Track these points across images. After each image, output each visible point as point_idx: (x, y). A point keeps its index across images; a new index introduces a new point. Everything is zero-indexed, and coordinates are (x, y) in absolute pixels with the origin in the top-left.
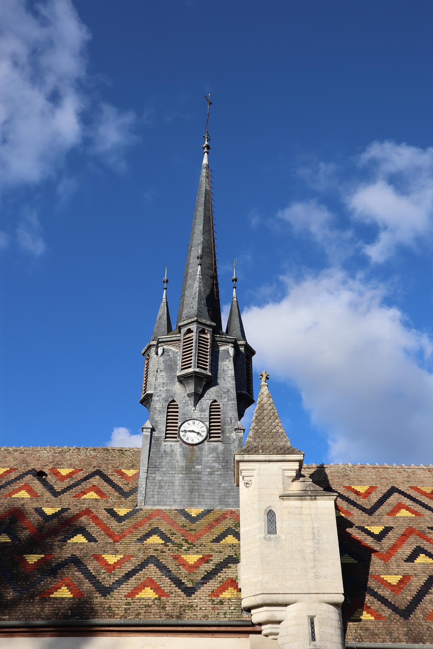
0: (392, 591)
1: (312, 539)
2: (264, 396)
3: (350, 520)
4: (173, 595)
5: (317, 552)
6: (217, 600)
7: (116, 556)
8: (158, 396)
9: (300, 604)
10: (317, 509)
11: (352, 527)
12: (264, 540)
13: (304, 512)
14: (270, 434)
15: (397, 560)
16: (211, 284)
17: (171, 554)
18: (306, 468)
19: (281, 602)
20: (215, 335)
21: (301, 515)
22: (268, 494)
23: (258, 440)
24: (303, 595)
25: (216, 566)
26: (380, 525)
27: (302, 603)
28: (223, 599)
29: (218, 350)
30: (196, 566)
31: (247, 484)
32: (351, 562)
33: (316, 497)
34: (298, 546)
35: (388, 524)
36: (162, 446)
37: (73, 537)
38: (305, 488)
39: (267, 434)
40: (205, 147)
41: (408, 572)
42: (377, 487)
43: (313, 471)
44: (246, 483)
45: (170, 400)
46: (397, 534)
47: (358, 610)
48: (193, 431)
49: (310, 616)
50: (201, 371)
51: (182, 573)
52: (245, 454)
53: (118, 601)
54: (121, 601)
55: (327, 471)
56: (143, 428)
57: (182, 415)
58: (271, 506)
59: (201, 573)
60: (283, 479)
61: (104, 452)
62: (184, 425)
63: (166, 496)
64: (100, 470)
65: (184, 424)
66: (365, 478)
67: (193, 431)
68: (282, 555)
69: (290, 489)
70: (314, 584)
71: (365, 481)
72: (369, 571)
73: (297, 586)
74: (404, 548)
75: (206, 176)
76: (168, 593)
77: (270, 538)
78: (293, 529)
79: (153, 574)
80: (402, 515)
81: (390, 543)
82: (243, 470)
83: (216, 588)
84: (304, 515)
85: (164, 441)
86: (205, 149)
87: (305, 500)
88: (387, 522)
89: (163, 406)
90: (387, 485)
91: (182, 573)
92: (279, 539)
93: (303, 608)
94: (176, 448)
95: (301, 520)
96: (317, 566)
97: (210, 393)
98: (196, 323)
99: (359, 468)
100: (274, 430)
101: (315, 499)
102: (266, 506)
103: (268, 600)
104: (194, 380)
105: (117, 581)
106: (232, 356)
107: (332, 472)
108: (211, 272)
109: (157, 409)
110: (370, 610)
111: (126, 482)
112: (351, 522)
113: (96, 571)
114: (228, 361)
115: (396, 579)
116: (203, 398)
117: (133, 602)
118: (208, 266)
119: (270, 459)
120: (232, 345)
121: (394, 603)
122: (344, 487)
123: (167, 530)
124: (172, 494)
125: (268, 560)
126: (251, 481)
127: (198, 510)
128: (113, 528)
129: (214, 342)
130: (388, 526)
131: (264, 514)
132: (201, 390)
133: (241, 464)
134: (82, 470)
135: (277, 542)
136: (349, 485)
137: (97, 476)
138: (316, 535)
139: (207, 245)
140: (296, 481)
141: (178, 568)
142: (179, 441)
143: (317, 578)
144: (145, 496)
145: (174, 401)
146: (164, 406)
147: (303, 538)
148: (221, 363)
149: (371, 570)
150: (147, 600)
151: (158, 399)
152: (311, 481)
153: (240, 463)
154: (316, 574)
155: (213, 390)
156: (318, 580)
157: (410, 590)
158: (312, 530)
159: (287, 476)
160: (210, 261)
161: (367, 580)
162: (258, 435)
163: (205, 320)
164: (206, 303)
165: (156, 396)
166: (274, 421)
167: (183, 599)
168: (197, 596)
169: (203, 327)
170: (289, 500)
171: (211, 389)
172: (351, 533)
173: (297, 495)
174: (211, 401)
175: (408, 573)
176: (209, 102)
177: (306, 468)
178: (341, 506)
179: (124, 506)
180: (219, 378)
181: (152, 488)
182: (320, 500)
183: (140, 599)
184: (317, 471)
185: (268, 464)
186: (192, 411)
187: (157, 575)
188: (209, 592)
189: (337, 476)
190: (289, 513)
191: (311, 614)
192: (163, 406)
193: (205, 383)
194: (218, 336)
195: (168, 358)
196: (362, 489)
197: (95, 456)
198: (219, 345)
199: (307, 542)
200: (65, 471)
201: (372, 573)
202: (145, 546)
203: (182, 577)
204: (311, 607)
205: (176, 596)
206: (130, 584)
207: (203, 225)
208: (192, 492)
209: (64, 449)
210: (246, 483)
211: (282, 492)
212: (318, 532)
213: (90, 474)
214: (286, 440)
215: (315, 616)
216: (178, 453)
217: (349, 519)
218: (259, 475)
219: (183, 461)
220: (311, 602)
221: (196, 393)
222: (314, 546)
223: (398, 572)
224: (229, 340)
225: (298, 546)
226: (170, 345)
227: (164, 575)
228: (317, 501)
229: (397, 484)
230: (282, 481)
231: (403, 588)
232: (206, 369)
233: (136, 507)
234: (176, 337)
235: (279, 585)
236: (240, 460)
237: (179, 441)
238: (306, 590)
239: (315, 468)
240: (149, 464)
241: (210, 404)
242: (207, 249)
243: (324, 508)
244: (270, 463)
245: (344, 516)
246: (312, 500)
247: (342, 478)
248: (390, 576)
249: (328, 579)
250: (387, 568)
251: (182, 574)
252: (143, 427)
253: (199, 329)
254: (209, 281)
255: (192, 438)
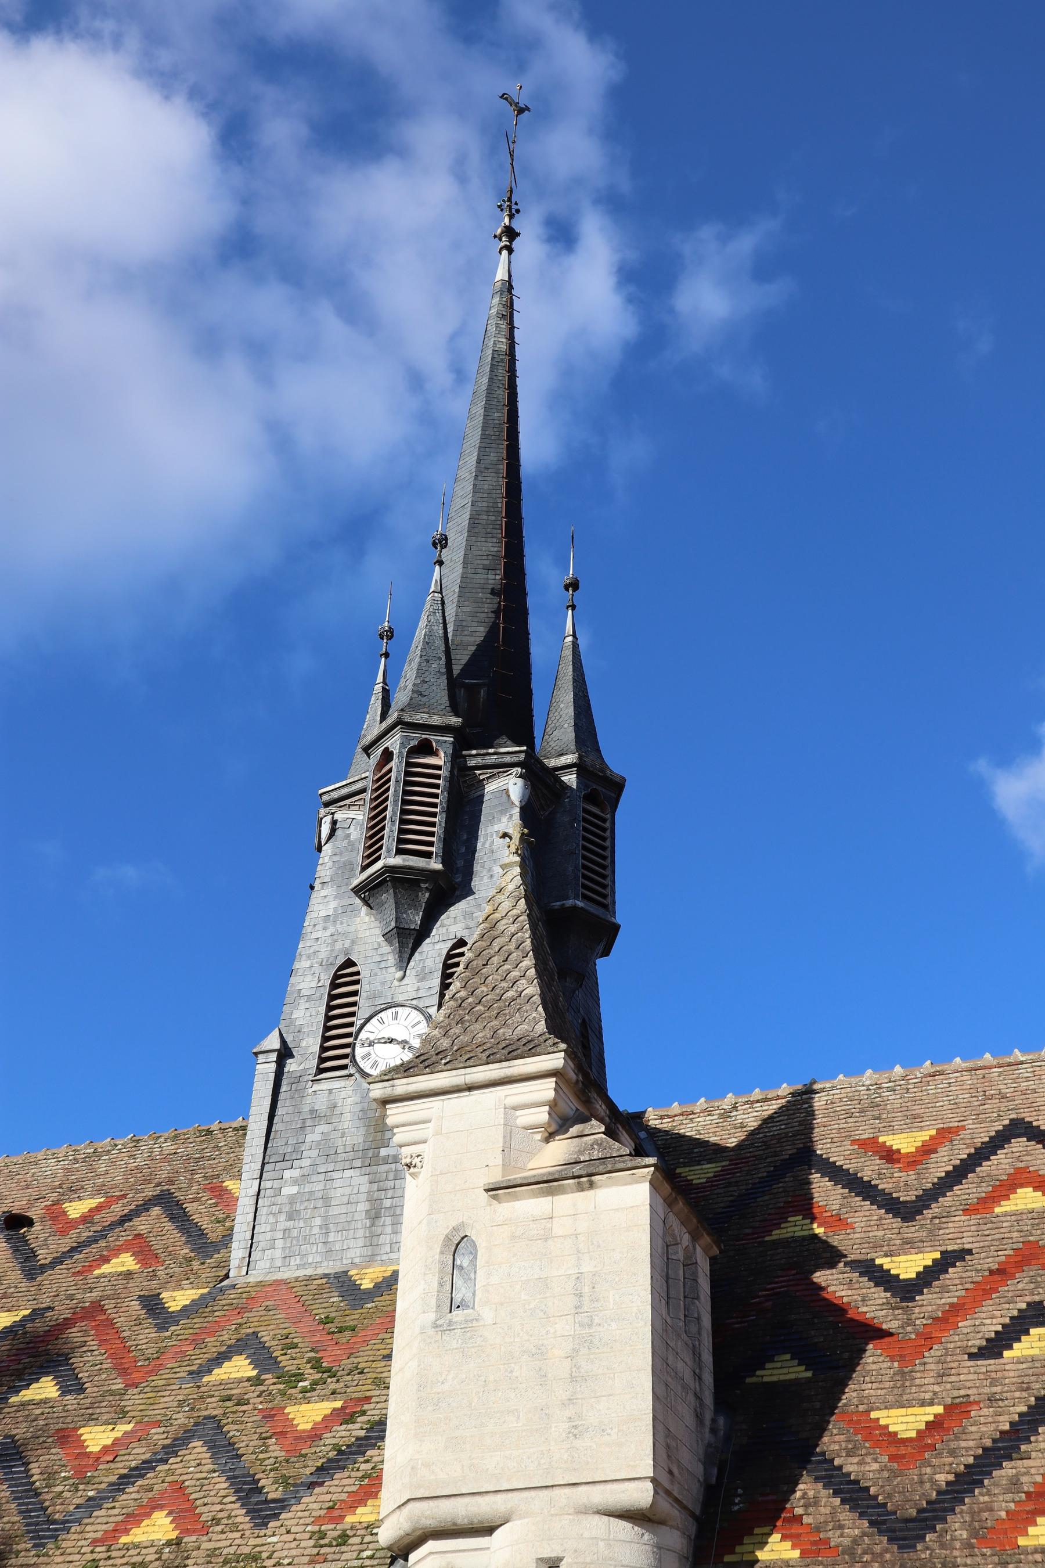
0: (892, 1458)
1: (573, 1311)
2: (503, 897)
3: (835, 1244)
4: (219, 1528)
5: (584, 1351)
6: (332, 1531)
7: (114, 1429)
8: (309, 957)
9: (519, 1522)
10: (596, 1214)
11: (832, 1265)
12: (431, 1332)
13: (558, 1230)
14: (495, 1005)
15: (946, 1354)
16: (492, 612)
17: (260, 1407)
18: (758, 1101)
19: (466, 1521)
20: (464, 753)
21: (546, 1240)
22: (458, 1188)
23: (457, 1030)
24: (533, 1493)
25: (368, 1430)
26: (929, 1249)
27: (526, 1520)
28: (352, 1529)
29: (479, 793)
30: (315, 1435)
31: (410, 1167)
32: (792, 1376)
33: (593, 1178)
34: (529, 1340)
35: (958, 1241)
36: (307, 1095)
37: (27, 1386)
38: (576, 1156)
39: (486, 1006)
40: (500, 235)
41: (969, 1392)
42: (963, 1128)
43: (775, 1107)
44: (407, 1165)
45: (341, 960)
46: (977, 1271)
47: (757, 1531)
48: (391, 1041)
49: (546, 1559)
50: (407, 863)
51: (269, 1458)
52: (397, 1076)
53: (67, 1560)
54: (75, 1559)
55: (819, 1102)
56: (256, 1054)
57: (367, 998)
58: (462, 1225)
59: (320, 1454)
60: (504, 1137)
61: (198, 1139)
62: (368, 1027)
63: (305, 1239)
64: (169, 1190)
65: (368, 1025)
66: (933, 1105)
67: (391, 1041)
68: (480, 1372)
69: (530, 1166)
70: (565, 1456)
71: (928, 1115)
72: (840, 1400)
73: (515, 1464)
74: (983, 1315)
75: (498, 313)
76: (208, 1521)
77: (450, 1323)
78: (518, 1287)
79: (192, 1469)
80: (1014, 1208)
81: (943, 1301)
82: (398, 1127)
83: (344, 1496)
84: (556, 1239)
85: (312, 1081)
86: (504, 239)
87: (562, 1191)
88: (960, 1235)
89: (319, 981)
90: (999, 1116)
91: (269, 1458)
92: (475, 1324)
93: (527, 1535)
94: (343, 1095)
95: (545, 1255)
96: (580, 1397)
97: (446, 922)
98: (401, 728)
99: (926, 1076)
100: (511, 994)
101: (591, 1185)
102: (448, 1227)
103: (426, 1518)
104: (391, 891)
105: (90, 1499)
106: (517, 803)
107: (832, 1103)
108: (493, 577)
109: (304, 992)
110: (796, 1529)
111: (223, 1213)
112: (839, 1251)
113: (45, 1476)
114: (505, 819)
115: (919, 1418)
116: (428, 941)
117: (105, 1559)
118: (487, 562)
119: (467, 1082)
120: (519, 769)
121: (885, 1498)
122: (854, 1142)
123: (279, 1336)
124: (323, 1232)
125: (438, 1393)
126: (420, 1155)
127: (384, 1269)
128: (139, 1347)
129: (467, 773)
130: (956, 1247)
131: (442, 1253)
132: (418, 919)
133: (392, 1109)
134: (124, 1196)
135: (469, 1334)
136: (872, 1136)
137: (156, 1208)
138: (586, 1300)
139: (485, 504)
140: (557, 1138)
141: (262, 1446)
142: (351, 1075)
143: (575, 1435)
144: (249, 1246)
145: (350, 963)
146: (322, 982)
147: (545, 1313)
148: (486, 831)
149: (850, 1395)
150: (143, 1550)
151: (308, 964)
152: (600, 1131)
153: (387, 1106)
154: (574, 1424)
155: (457, 911)
156: (578, 1443)
157: (953, 1453)
158: (574, 1283)
159: (523, 1125)
160: (492, 549)
161: (821, 1429)
162: (459, 1014)
163: (426, 716)
164: (444, 666)
165: (304, 958)
166: (515, 966)
167: (241, 1538)
168: (282, 1526)
169: (424, 736)
170: (516, 1198)
171: (452, 908)
172: (823, 1284)
173: (533, 1180)
174: (449, 944)
175: (968, 1395)
176: (516, 106)
177: (758, 1101)
178: (824, 1203)
179: (191, 1283)
180: (476, 875)
181: (272, 1220)
182: (607, 1186)
183: (127, 1548)
184: (789, 1104)
185: (466, 1098)
186: (396, 983)
187: (201, 1472)
188: (321, 1509)
189: (843, 1112)
190: (513, 1237)
191: (548, 1553)
192: (319, 981)
193: (427, 895)
194: (474, 752)
195: (345, 843)
196: (904, 1142)
197: (171, 1154)
198: (484, 780)
199: (556, 1324)
200: (81, 1207)
201: (845, 1405)
202: (202, 1389)
203: (263, 1472)
204: (549, 1529)
205: (225, 1530)
206: (120, 1505)
207: (479, 451)
208: (377, 1216)
209: (101, 1148)
210: (407, 1165)
211: (496, 1176)
212: (593, 1288)
213: (140, 1205)
214: (534, 1017)
215: (560, 1559)
216: (347, 1109)
217: (835, 1241)
218: (438, 1133)
219: (358, 1132)
220: (552, 1515)
221: (403, 928)
222: (577, 1333)
223: (935, 1393)
224: (507, 759)
225: (529, 1340)
226: (352, 808)
227: (218, 1471)
228: (598, 1191)
229: (1032, 1109)
230: (502, 1145)
231: (932, 1447)
232: (428, 855)
233: (222, 1281)
234: (363, 781)
235: (463, 1466)
236: (384, 1096)
237: (351, 1075)
238: (541, 1476)
239: (785, 1097)
240: (268, 1152)
241: (444, 952)
242: (485, 517)
243: (617, 1210)
244: (472, 1093)
245: (820, 1235)
246: (581, 1188)
247: (858, 1114)
248: (903, 1411)
249: (609, 1434)
250: (903, 1386)
251: (266, 1462)
252: (255, 1050)
253: (409, 744)
254: (486, 605)
255: (386, 1061)
